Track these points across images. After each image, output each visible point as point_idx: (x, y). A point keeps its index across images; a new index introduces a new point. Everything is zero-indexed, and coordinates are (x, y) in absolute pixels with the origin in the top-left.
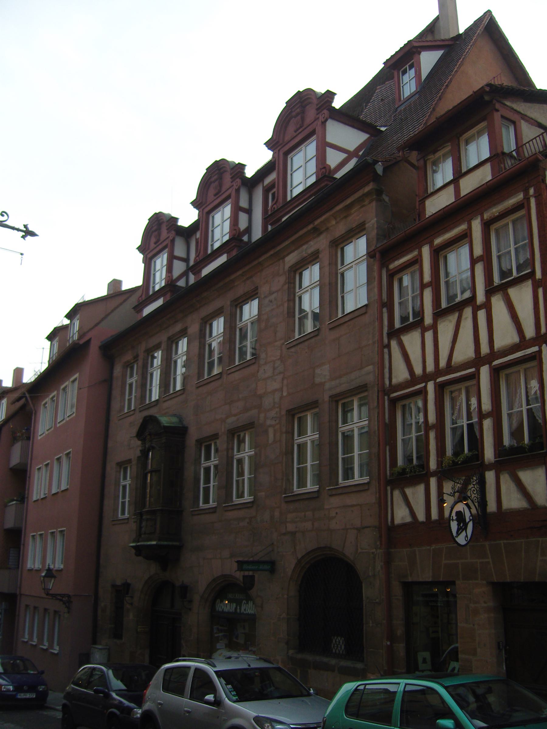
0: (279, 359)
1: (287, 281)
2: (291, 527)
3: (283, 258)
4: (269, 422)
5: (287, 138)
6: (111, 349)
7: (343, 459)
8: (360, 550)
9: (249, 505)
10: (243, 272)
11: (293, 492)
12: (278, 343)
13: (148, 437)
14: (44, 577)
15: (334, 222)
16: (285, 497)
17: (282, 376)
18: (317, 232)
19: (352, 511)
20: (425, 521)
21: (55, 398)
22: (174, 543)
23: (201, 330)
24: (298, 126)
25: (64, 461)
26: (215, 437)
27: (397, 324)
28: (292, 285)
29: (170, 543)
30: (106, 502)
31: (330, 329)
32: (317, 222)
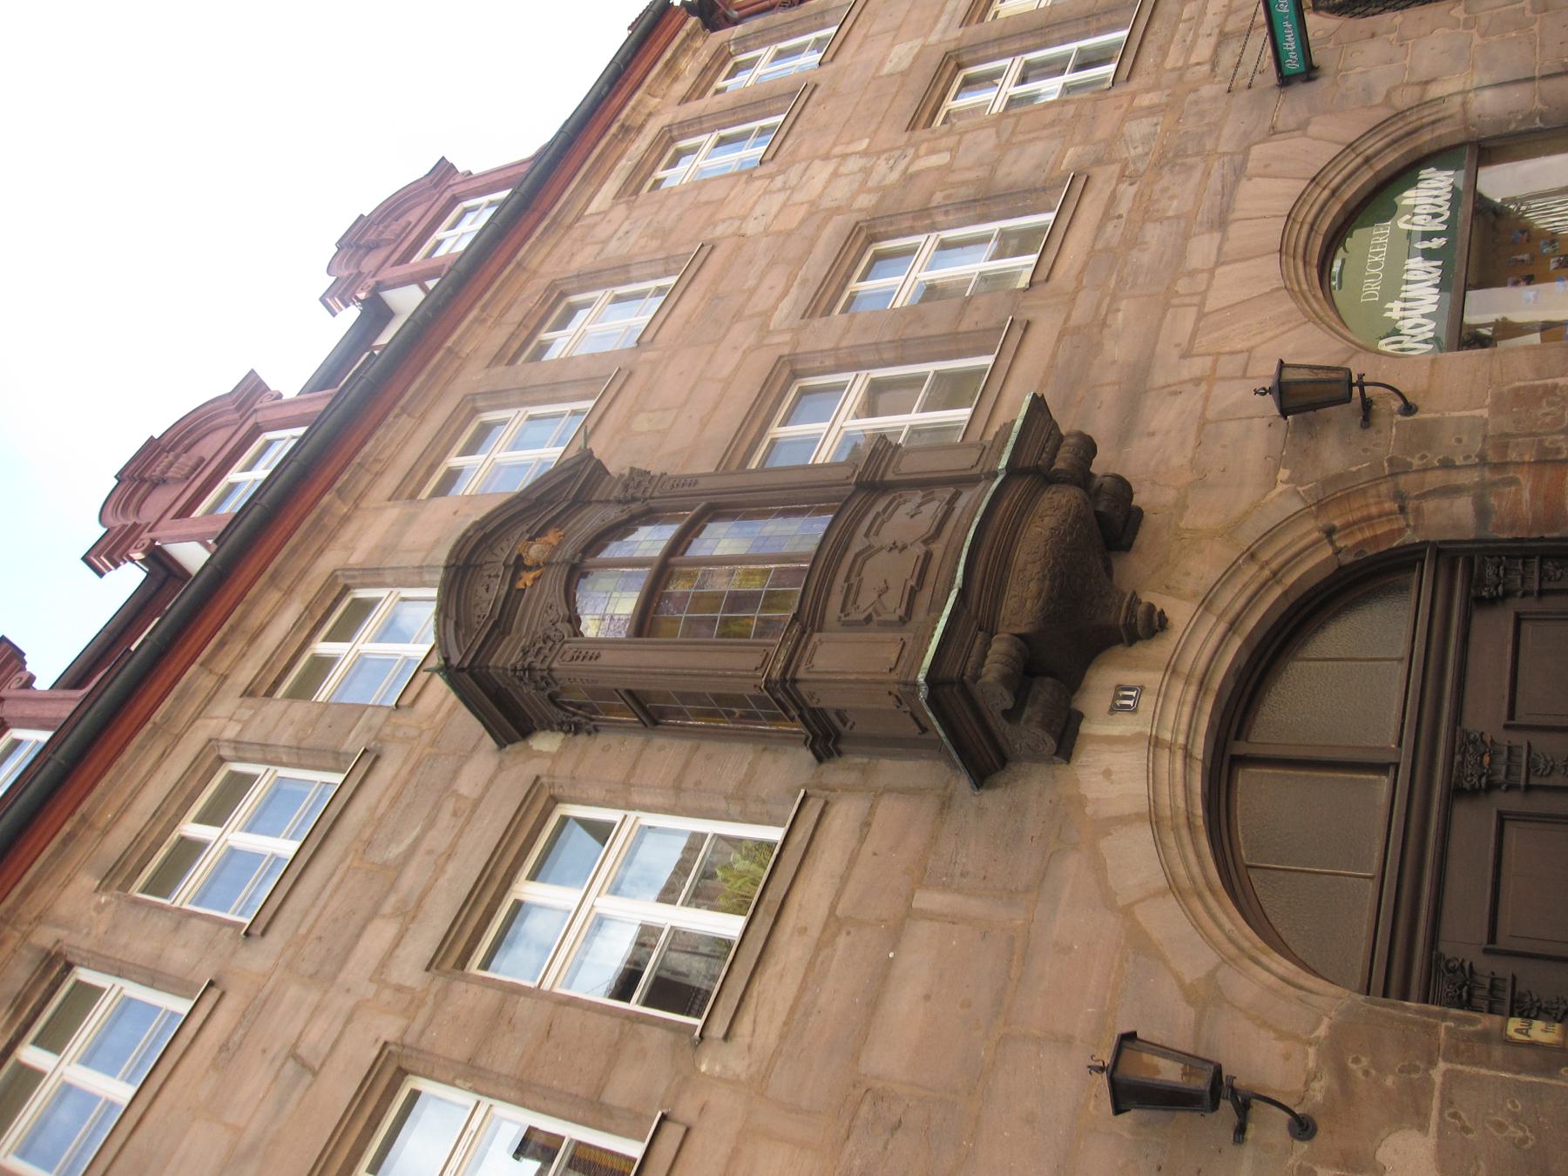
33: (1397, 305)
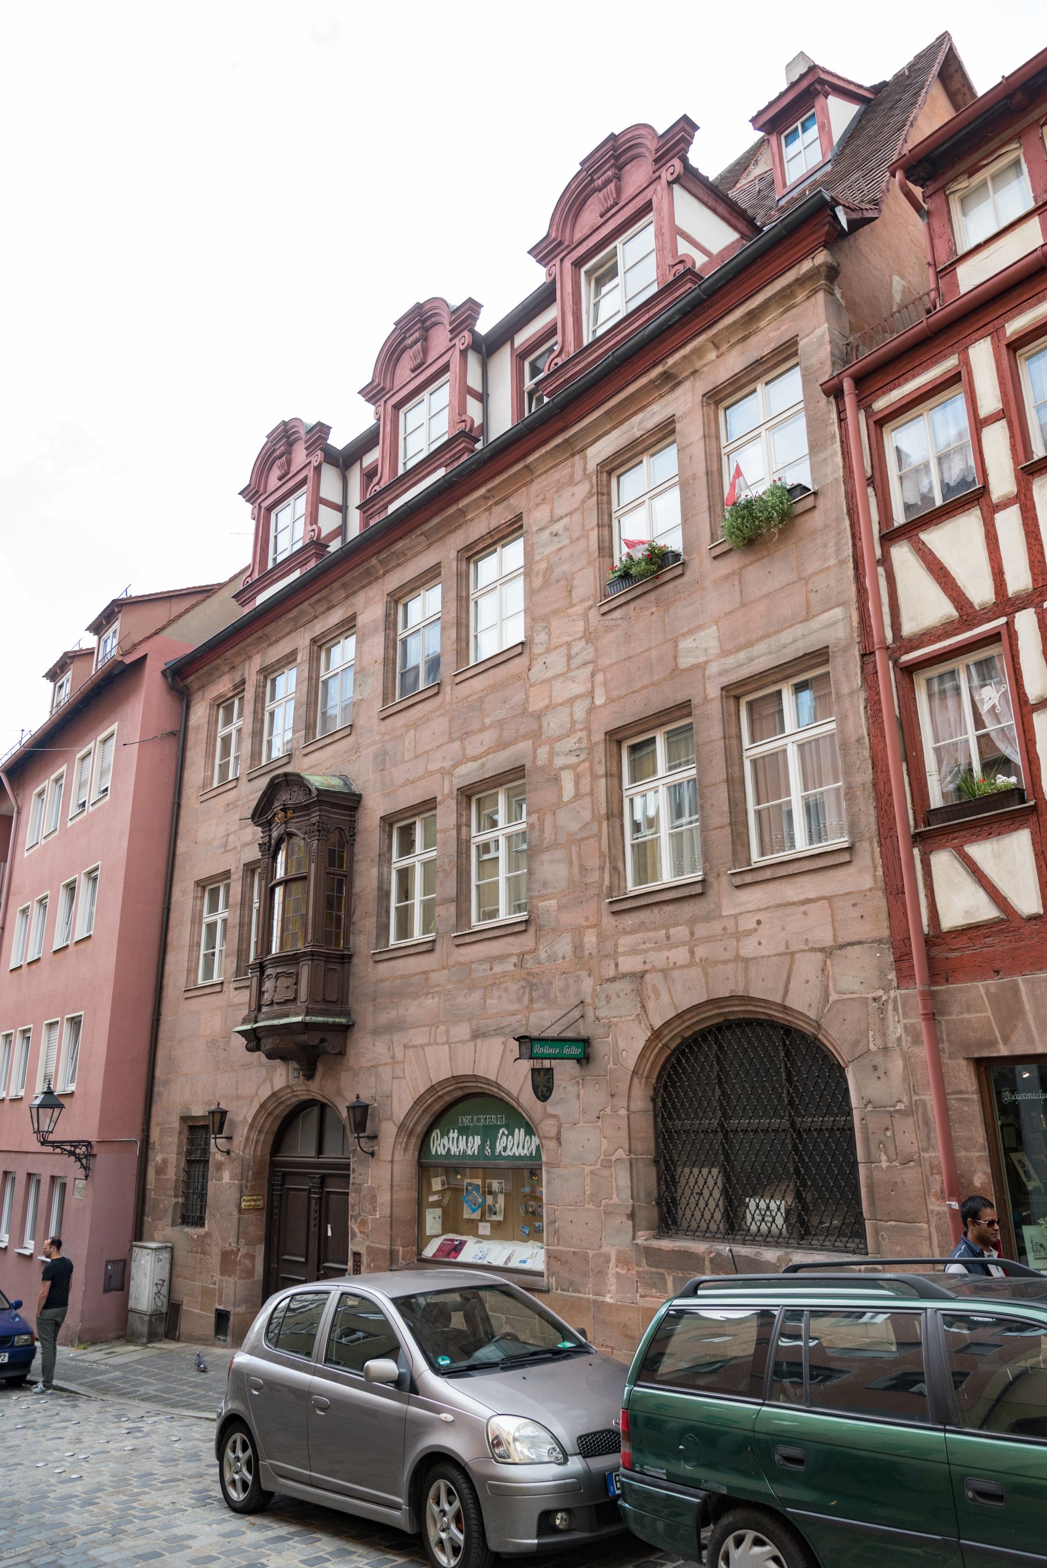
0: (580, 639)
1: (595, 490)
2: (629, 964)
3: (583, 450)
4: (559, 761)
5: (578, 236)
6: (183, 677)
7: (759, 813)
8: (833, 997)
9: (518, 929)
10: (488, 491)
11: (625, 894)
12: (579, 609)
13: (281, 815)
14: (40, 1106)
15: (712, 355)
16: (610, 903)
17: (590, 668)
18: (670, 381)
19: (805, 913)
20: (1042, 912)
21: (63, 781)
22: (337, 1020)
23: (387, 615)
24: (610, 202)
25: (83, 889)
26: (428, 805)
27: (899, 518)
28: (605, 498)
29: (330, 1020)
30: (170, 957)
31: (715, 558)
32: (671, 361)
33: (456, 1135)
